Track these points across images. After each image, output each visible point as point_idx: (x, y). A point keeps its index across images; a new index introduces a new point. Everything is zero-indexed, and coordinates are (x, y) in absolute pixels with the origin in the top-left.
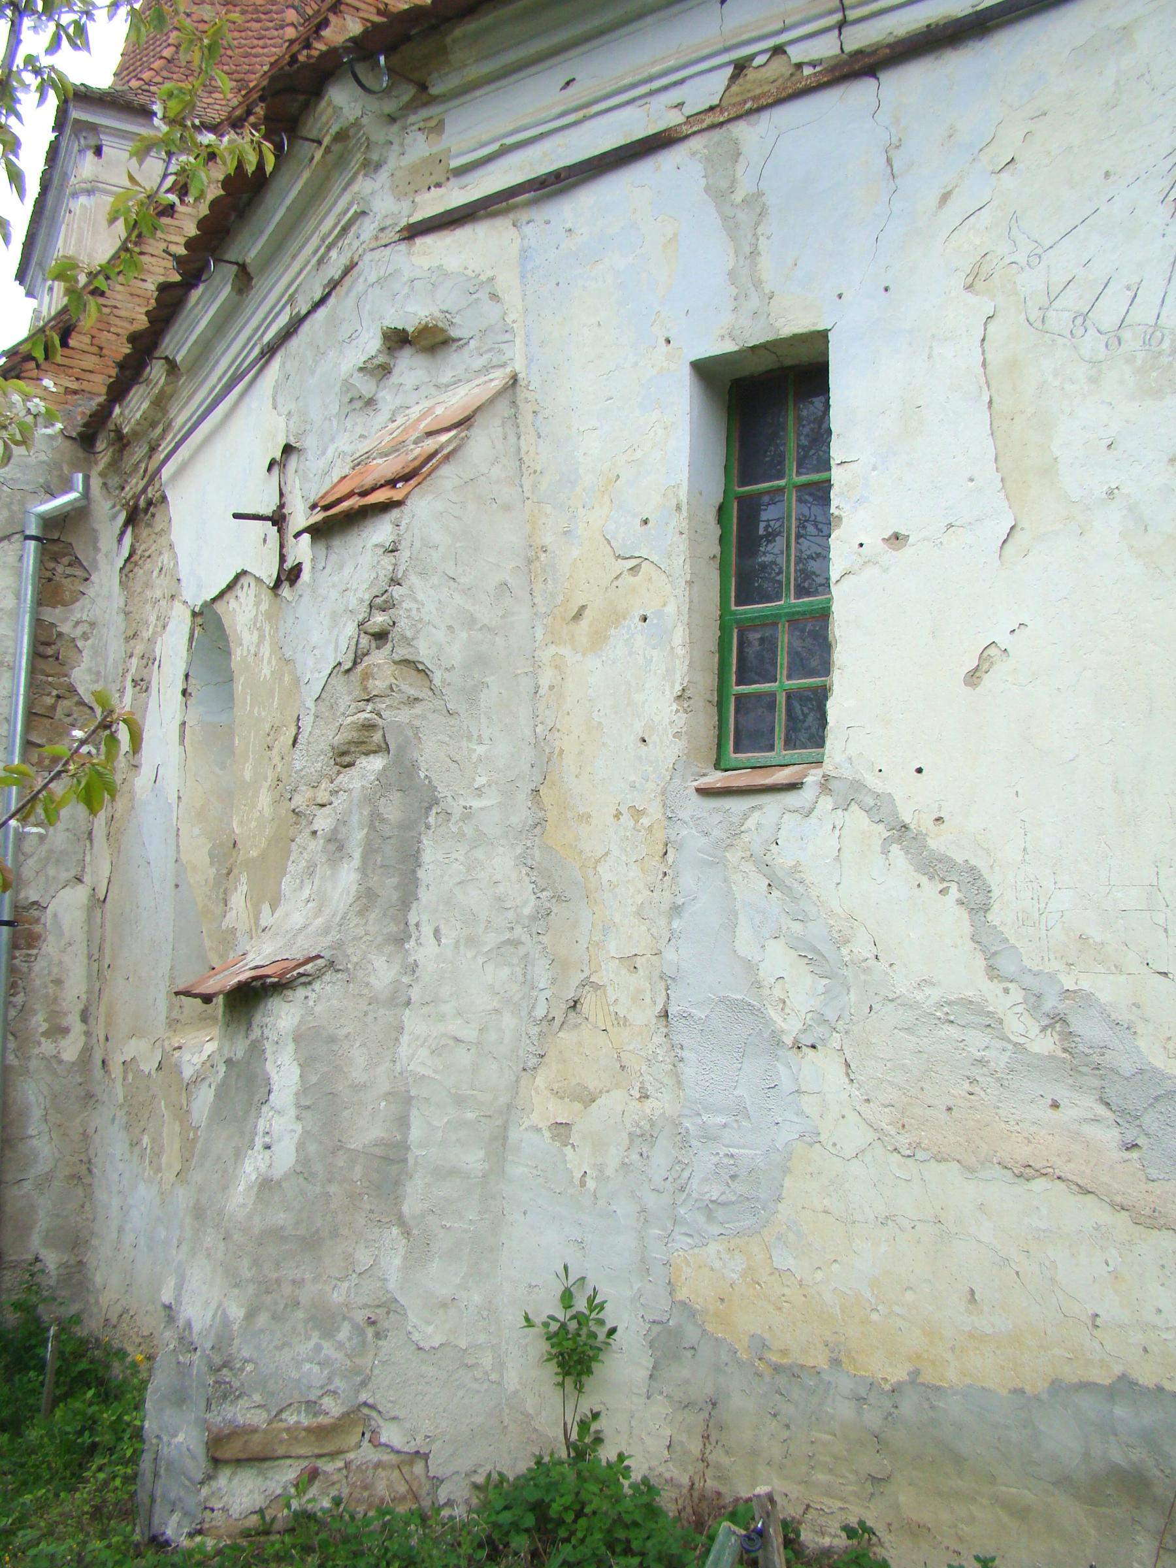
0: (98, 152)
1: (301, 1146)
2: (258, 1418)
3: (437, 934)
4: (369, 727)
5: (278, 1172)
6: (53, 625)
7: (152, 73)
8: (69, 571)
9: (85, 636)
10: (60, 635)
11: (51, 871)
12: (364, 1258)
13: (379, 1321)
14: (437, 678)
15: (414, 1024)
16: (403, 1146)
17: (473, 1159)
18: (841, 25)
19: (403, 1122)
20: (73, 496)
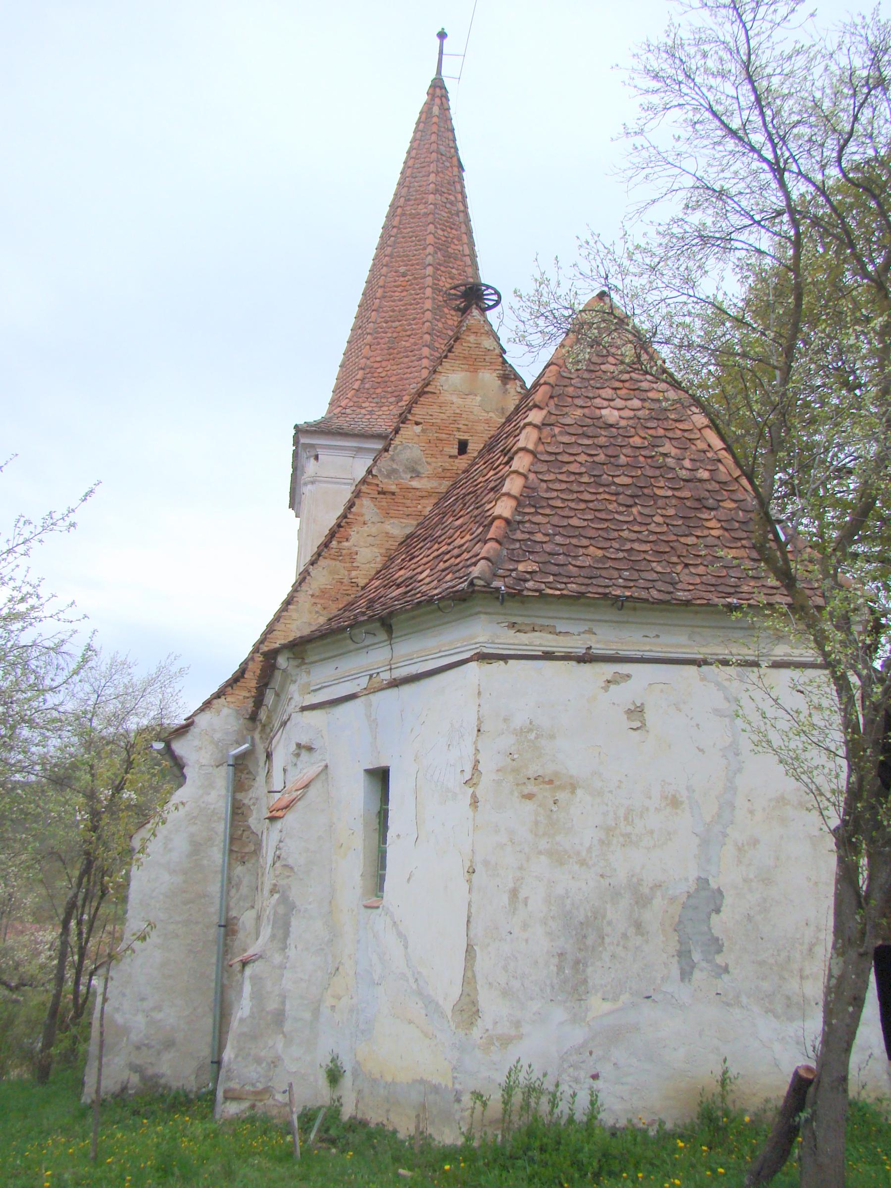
0: (317, 458)
1: (251, 1009)
2: (237, 1087)
3: (296, 947)
4: (275, 885)
5: (245, 1016)
6: (241, 800)
7: (347, 400)
8: (247, 776)
9: (254, 804)
10: (244, 804)
11: (241, 903)
12: (271, 1043)
13: (275, 1063)
14: (296, 869)
15: (287, 974)
16: (284, 1010)
17: (307, 1015)
18: (391, 669)
19: (283, 1003)
20: (247, 745)
